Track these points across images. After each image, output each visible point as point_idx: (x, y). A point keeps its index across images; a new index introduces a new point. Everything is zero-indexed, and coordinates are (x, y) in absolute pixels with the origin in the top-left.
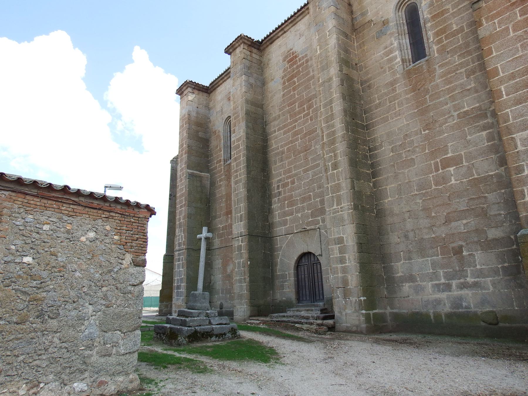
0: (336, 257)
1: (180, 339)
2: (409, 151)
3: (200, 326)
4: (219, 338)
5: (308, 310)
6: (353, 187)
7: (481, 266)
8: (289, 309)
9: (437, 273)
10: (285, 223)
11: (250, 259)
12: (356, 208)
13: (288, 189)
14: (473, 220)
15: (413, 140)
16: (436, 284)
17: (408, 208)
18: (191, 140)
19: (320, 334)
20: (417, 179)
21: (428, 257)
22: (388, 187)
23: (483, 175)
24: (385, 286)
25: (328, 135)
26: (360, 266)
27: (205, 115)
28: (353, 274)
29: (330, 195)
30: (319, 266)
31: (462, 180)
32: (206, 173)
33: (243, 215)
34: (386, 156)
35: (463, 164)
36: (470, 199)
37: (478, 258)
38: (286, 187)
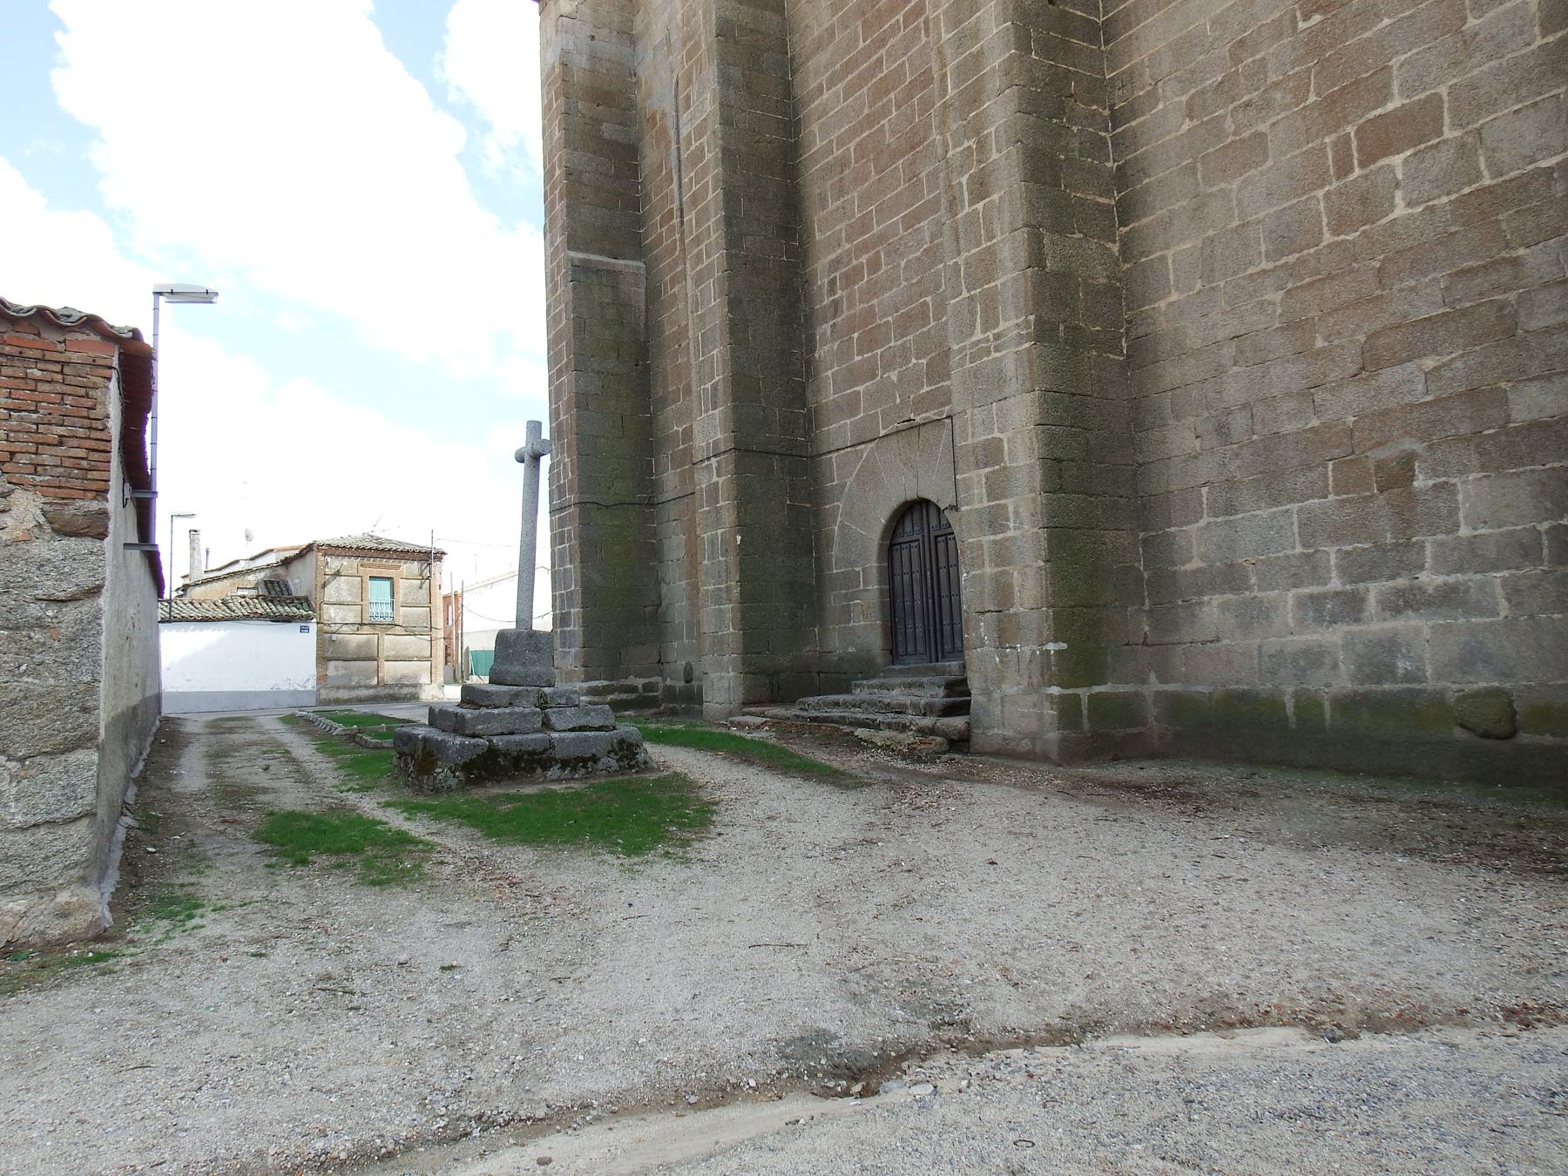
0: (977, 510)
1: (441, 772)
2: (1248, 104)
3: (512, 733)
4: (574, 769)
5: (910, 686)
6: (1037, 258)
7: (1475, 529)
8: (858, 682)
9: (1319, 555)
10: (852, 405)
11: (742, 526)
12: (1043, 333)
14: (1462, 356)
15: (1263, 59)
16: (1311, 597)
18: (576, 149)
19: (919, 760)
20: (1272, 211)
21: (1292, 501)
22: (1170, 253)
23: (1513, 174)
24: (1147, 607)
25: (963, 71)
26: (1049, 539)
27: (619, 64)
30: (951, 543)
31: (1435, 202)
32: (634, 259)
33: (720, 386)
34: (1170, 132)
35: (1440, 133)
36: (1456, 274)
37: (1466, 499)
38: (855, 282)
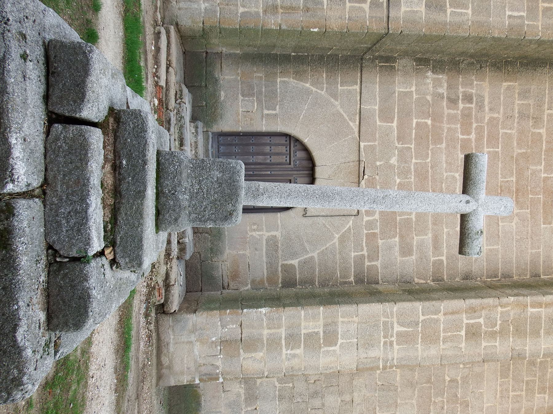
2: (443, 408)
13: (455, 130)
17: (357, 400)
28: (265, 364)
29: (422, 318)
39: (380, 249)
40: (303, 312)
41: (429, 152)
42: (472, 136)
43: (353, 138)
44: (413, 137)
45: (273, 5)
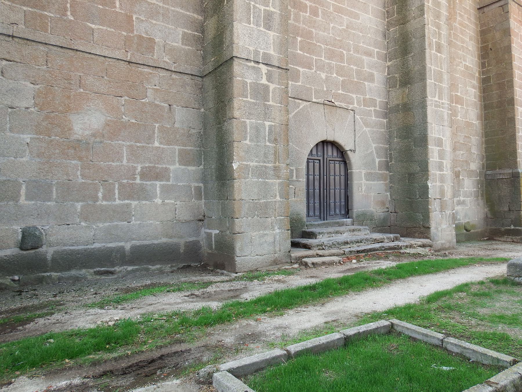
39: (371, 97)
40: (431, 159)
41: (318, 44)
42: (308, 4)
43: (310, 107)
44: (308, 55)
45: (274, 170)
